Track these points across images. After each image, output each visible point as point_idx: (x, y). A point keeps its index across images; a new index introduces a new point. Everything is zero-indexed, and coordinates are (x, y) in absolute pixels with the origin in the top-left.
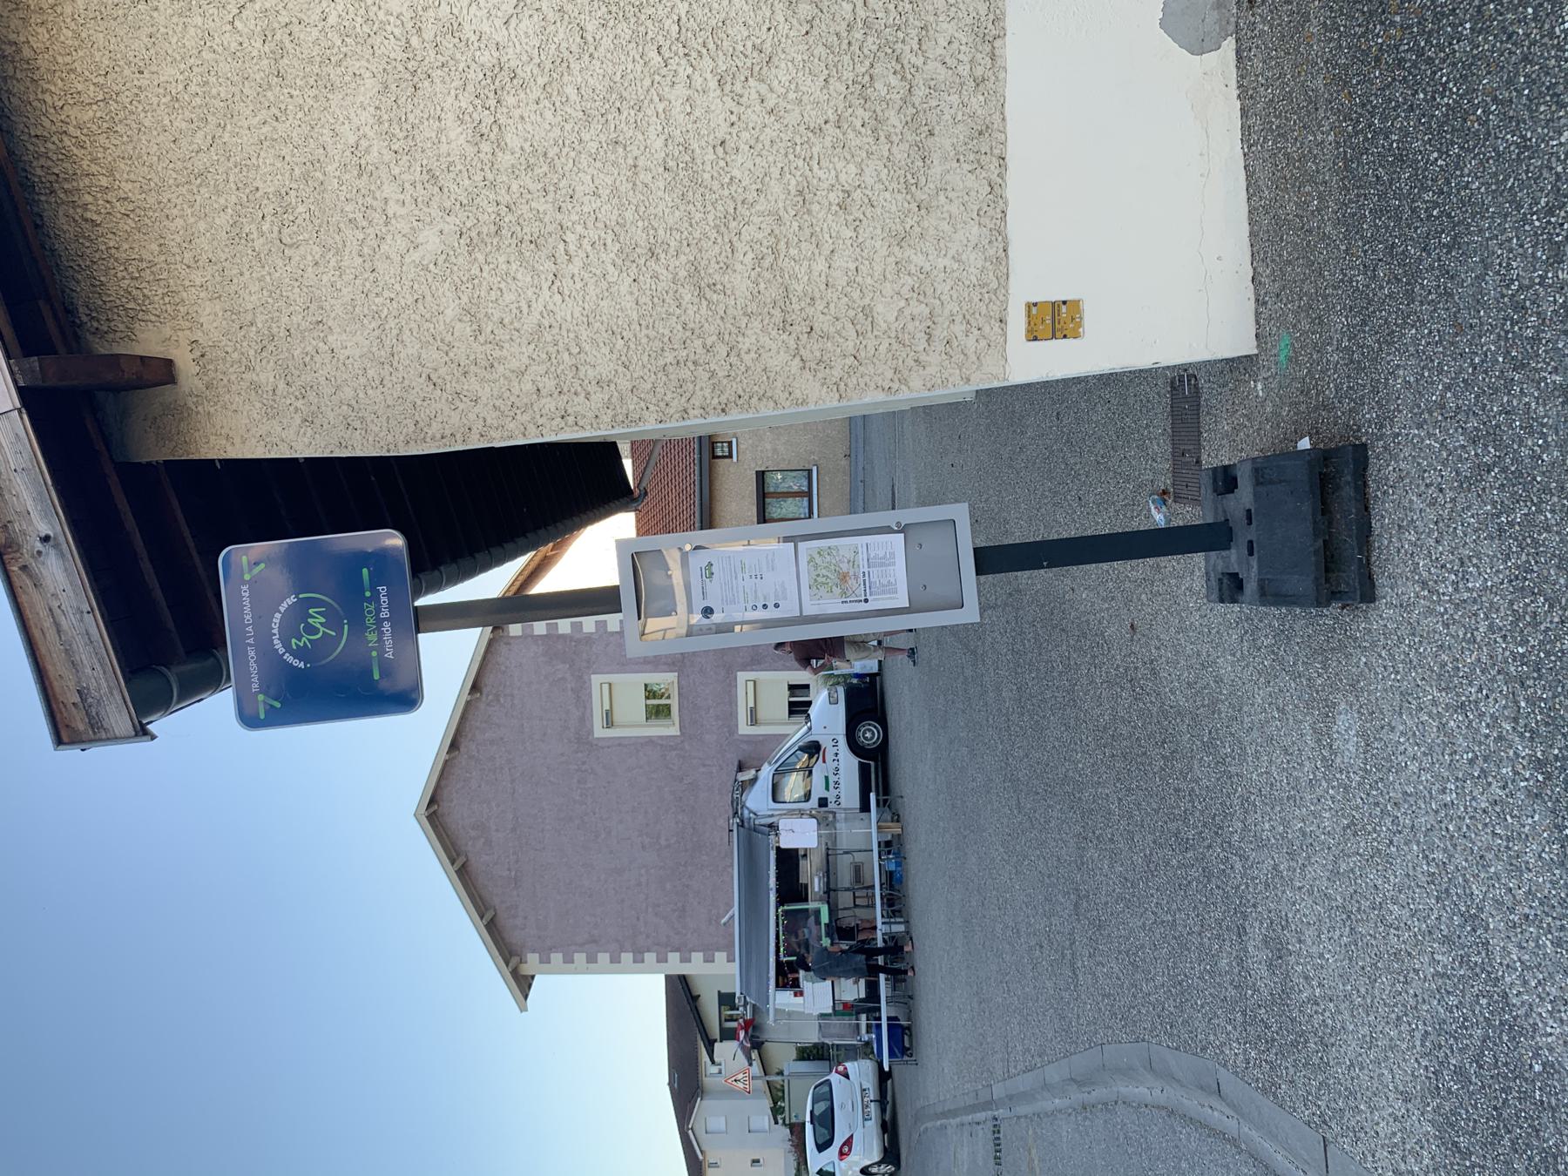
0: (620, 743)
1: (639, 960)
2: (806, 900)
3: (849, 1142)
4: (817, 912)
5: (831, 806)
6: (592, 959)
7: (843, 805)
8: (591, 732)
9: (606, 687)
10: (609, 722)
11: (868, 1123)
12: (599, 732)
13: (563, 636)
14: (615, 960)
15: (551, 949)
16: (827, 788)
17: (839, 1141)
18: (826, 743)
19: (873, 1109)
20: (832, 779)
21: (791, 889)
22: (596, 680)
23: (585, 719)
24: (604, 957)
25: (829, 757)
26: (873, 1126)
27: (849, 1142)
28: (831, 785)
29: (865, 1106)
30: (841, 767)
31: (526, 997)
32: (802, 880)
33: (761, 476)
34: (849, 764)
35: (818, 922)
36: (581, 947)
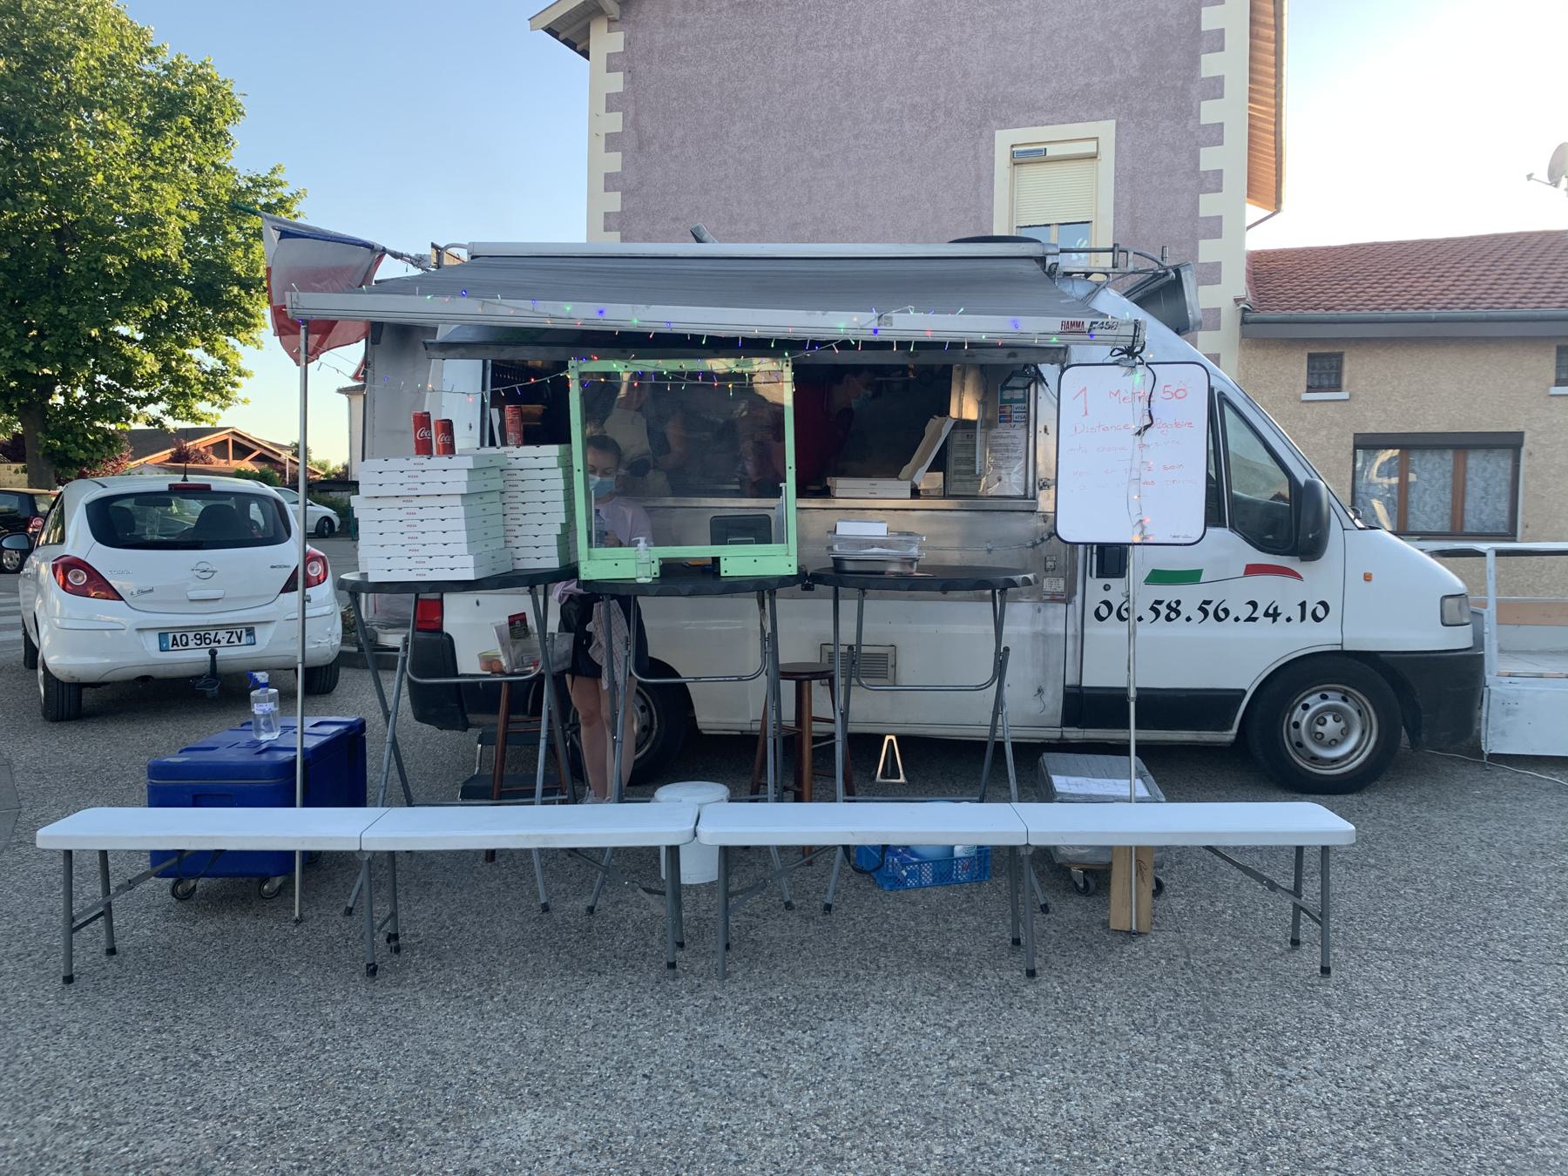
0: (983, 180)
1: (611, 182)
2: (801, 493)
3: (98, 585)
4: (759, 530)
5: (1095, 590)
6: (612, 142)
7: (1093, 628)
8: (1006, 124)
9: (1089, 148)
10: (1024, 158)
11: (152, 641)
12: (1005, 140)
13: (1195, 62)
14: (611, 182)
15: (631, 75)
16: (1157, 577)
17: (105, 559)
18: (1317, 580)
19: (193, 657)
20: (1190, 597)
21: (872, 410)
22: (1105, 130)
23: (1031, 112)
24: (614, 162)
25: (1267, 589)
26: (146, 655)
27: (98, 585)
28: (1168, 593)
29: (203, 635)
30: (1228, 629)
31: (549, 30)
32: (841, 485)
33: (1511, 443)
34: (1234, 658)
35: (728, 530)
36: (633, 123)
